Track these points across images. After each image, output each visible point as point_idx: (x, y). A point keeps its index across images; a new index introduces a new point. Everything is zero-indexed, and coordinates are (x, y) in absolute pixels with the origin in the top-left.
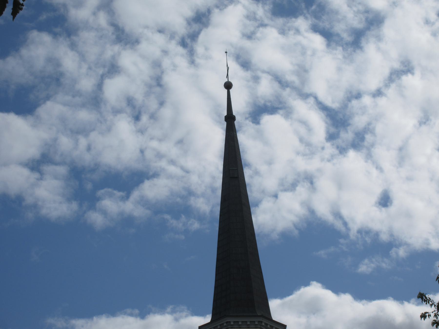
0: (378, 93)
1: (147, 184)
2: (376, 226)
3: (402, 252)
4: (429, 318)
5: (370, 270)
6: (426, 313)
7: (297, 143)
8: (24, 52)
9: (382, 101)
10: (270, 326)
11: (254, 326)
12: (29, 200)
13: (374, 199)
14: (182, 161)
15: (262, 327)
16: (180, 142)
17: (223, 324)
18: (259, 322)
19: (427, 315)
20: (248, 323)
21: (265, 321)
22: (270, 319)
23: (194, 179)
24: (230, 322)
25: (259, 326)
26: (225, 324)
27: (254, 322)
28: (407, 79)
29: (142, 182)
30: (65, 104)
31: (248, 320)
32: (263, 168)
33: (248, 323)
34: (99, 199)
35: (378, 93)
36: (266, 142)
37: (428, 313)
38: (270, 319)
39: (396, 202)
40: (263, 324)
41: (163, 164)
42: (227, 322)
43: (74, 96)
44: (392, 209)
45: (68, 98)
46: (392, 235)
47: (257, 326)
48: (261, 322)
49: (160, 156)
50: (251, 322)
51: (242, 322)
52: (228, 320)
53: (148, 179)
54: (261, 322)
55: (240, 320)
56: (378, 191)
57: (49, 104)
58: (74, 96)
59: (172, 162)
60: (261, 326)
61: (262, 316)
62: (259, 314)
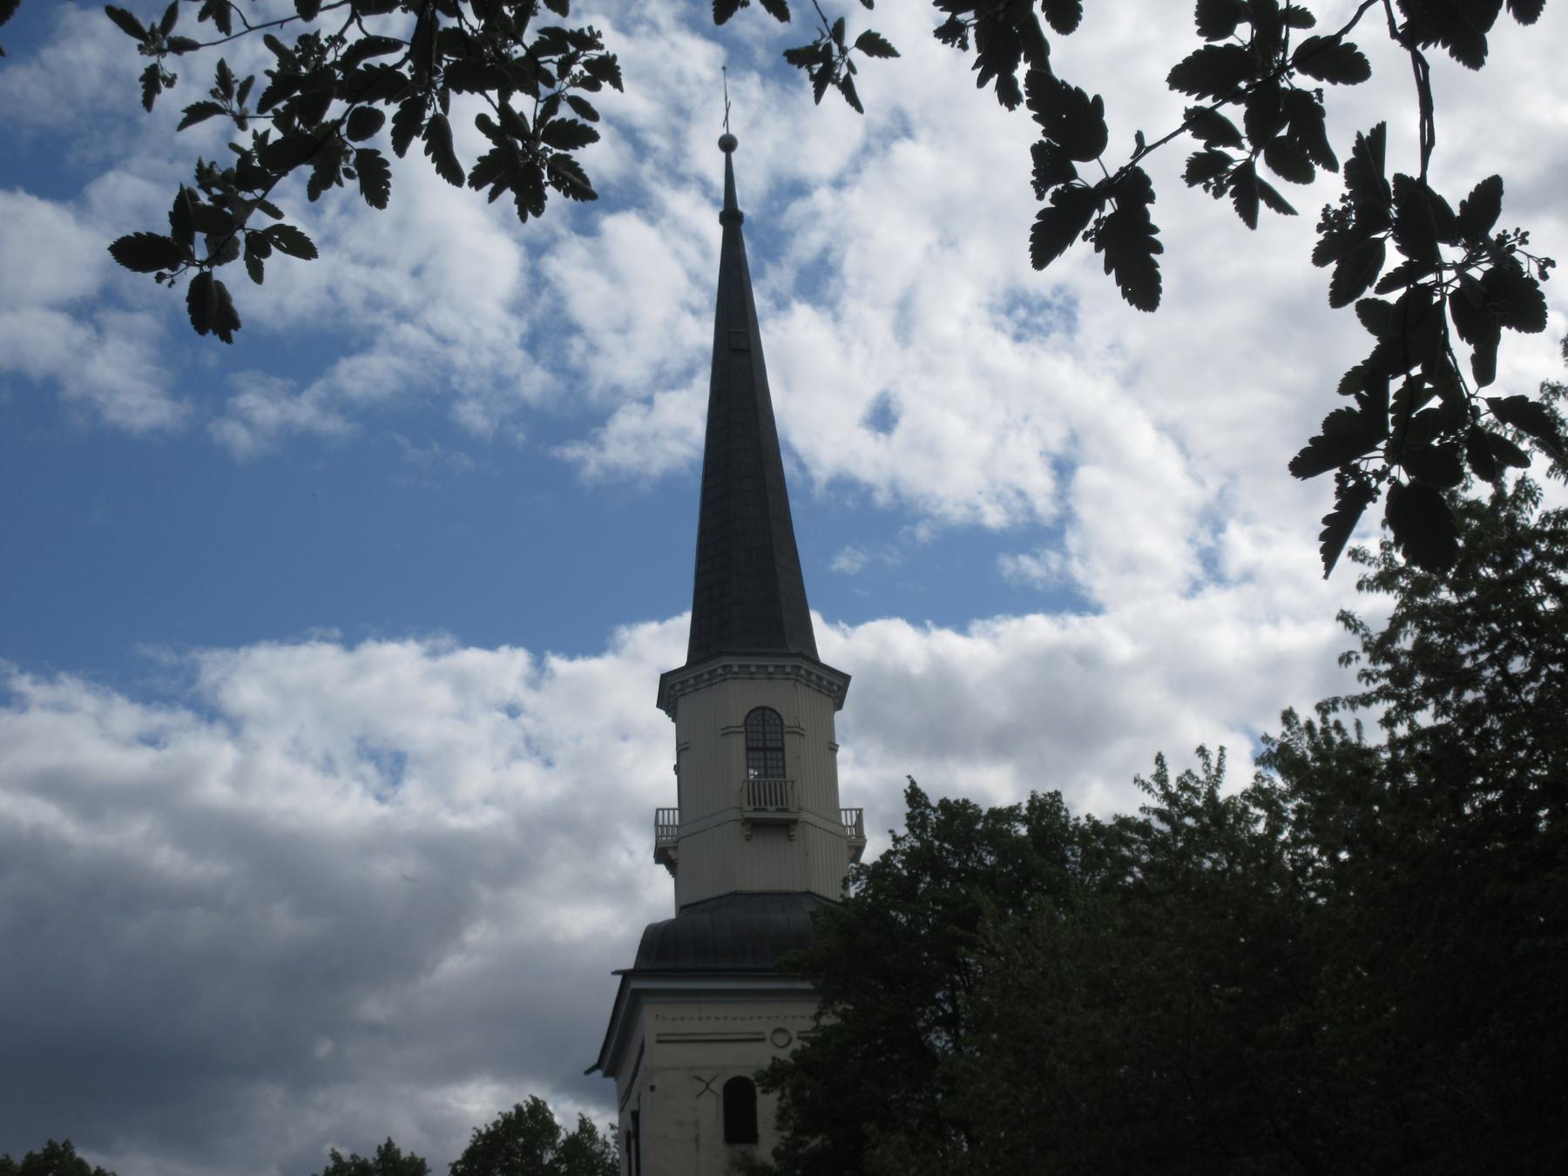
0: (838, 184)
1: (345, 366)
2: (865, 472)
3: (923, 532)
4: (1357, 662)
5: (858, 566)
6: (1351, 652)
7: (682, 281)
8: (48, 54)
9: (854, 198)
10: (818, 677)
11: (782, 677)
12: (73, 390)
13: (860, 409)
14: (430, 317)
15: (798, 678)
16: (417, 272)
17: (715, 670)
18: (793, 667)
19: (1353, 656)
20: (771, 670)
21: (805, 665)
22: (814, 660)
23: (461, 358)
24: (731, 666)
25: (794, 677)
26: (720, 671)
27: (748, 667)
28: (904, 151)
29: (333, 361)
30: (146, 177)
31: (771, 663)
32: (610, 341)
33: (771, 670)
34: (235, 392)
35: (838, 184)
36: (615, 277)
37: (1355, 652)
38: (811, 659)
39: (905, 422)
40: (803, 672)
41: (381, 318)
42: (724, 667)
43: (171, 161)
44: (899, 434)
45: (159, 164)
46: (896, 495)
47: (788, 676)
48: (799, 668)
49: (374, 303)
50: (776, 667)
51: (740, 666)
52: (727, 661)
53: (349, 352)
54: (799, 668)
55: (753, 662)
56: (869, 391)
57: (111, 178)
58: (171, 161)
59: (403, 316)
60: (797, 676)
61: (800, 655)
62: (792, 652)
